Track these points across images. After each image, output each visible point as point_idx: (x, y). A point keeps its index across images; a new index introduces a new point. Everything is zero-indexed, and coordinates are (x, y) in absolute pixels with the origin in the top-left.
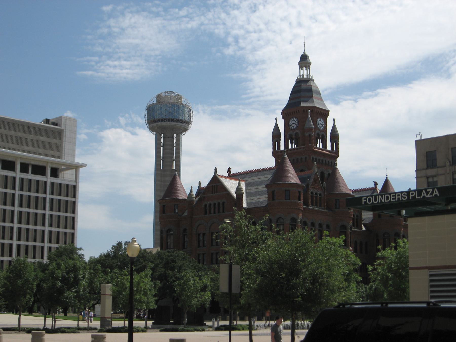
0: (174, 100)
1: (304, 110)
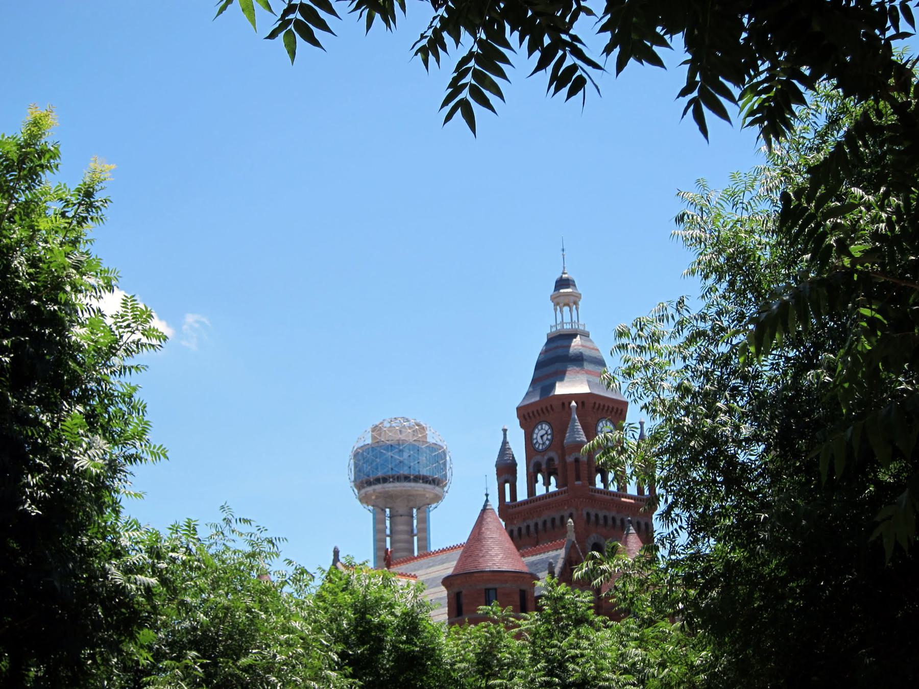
0: (408, 436)
1: (563, 404)
